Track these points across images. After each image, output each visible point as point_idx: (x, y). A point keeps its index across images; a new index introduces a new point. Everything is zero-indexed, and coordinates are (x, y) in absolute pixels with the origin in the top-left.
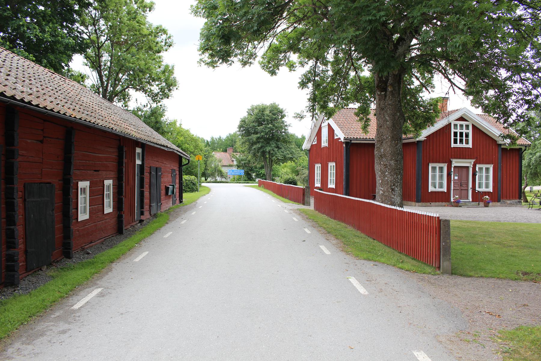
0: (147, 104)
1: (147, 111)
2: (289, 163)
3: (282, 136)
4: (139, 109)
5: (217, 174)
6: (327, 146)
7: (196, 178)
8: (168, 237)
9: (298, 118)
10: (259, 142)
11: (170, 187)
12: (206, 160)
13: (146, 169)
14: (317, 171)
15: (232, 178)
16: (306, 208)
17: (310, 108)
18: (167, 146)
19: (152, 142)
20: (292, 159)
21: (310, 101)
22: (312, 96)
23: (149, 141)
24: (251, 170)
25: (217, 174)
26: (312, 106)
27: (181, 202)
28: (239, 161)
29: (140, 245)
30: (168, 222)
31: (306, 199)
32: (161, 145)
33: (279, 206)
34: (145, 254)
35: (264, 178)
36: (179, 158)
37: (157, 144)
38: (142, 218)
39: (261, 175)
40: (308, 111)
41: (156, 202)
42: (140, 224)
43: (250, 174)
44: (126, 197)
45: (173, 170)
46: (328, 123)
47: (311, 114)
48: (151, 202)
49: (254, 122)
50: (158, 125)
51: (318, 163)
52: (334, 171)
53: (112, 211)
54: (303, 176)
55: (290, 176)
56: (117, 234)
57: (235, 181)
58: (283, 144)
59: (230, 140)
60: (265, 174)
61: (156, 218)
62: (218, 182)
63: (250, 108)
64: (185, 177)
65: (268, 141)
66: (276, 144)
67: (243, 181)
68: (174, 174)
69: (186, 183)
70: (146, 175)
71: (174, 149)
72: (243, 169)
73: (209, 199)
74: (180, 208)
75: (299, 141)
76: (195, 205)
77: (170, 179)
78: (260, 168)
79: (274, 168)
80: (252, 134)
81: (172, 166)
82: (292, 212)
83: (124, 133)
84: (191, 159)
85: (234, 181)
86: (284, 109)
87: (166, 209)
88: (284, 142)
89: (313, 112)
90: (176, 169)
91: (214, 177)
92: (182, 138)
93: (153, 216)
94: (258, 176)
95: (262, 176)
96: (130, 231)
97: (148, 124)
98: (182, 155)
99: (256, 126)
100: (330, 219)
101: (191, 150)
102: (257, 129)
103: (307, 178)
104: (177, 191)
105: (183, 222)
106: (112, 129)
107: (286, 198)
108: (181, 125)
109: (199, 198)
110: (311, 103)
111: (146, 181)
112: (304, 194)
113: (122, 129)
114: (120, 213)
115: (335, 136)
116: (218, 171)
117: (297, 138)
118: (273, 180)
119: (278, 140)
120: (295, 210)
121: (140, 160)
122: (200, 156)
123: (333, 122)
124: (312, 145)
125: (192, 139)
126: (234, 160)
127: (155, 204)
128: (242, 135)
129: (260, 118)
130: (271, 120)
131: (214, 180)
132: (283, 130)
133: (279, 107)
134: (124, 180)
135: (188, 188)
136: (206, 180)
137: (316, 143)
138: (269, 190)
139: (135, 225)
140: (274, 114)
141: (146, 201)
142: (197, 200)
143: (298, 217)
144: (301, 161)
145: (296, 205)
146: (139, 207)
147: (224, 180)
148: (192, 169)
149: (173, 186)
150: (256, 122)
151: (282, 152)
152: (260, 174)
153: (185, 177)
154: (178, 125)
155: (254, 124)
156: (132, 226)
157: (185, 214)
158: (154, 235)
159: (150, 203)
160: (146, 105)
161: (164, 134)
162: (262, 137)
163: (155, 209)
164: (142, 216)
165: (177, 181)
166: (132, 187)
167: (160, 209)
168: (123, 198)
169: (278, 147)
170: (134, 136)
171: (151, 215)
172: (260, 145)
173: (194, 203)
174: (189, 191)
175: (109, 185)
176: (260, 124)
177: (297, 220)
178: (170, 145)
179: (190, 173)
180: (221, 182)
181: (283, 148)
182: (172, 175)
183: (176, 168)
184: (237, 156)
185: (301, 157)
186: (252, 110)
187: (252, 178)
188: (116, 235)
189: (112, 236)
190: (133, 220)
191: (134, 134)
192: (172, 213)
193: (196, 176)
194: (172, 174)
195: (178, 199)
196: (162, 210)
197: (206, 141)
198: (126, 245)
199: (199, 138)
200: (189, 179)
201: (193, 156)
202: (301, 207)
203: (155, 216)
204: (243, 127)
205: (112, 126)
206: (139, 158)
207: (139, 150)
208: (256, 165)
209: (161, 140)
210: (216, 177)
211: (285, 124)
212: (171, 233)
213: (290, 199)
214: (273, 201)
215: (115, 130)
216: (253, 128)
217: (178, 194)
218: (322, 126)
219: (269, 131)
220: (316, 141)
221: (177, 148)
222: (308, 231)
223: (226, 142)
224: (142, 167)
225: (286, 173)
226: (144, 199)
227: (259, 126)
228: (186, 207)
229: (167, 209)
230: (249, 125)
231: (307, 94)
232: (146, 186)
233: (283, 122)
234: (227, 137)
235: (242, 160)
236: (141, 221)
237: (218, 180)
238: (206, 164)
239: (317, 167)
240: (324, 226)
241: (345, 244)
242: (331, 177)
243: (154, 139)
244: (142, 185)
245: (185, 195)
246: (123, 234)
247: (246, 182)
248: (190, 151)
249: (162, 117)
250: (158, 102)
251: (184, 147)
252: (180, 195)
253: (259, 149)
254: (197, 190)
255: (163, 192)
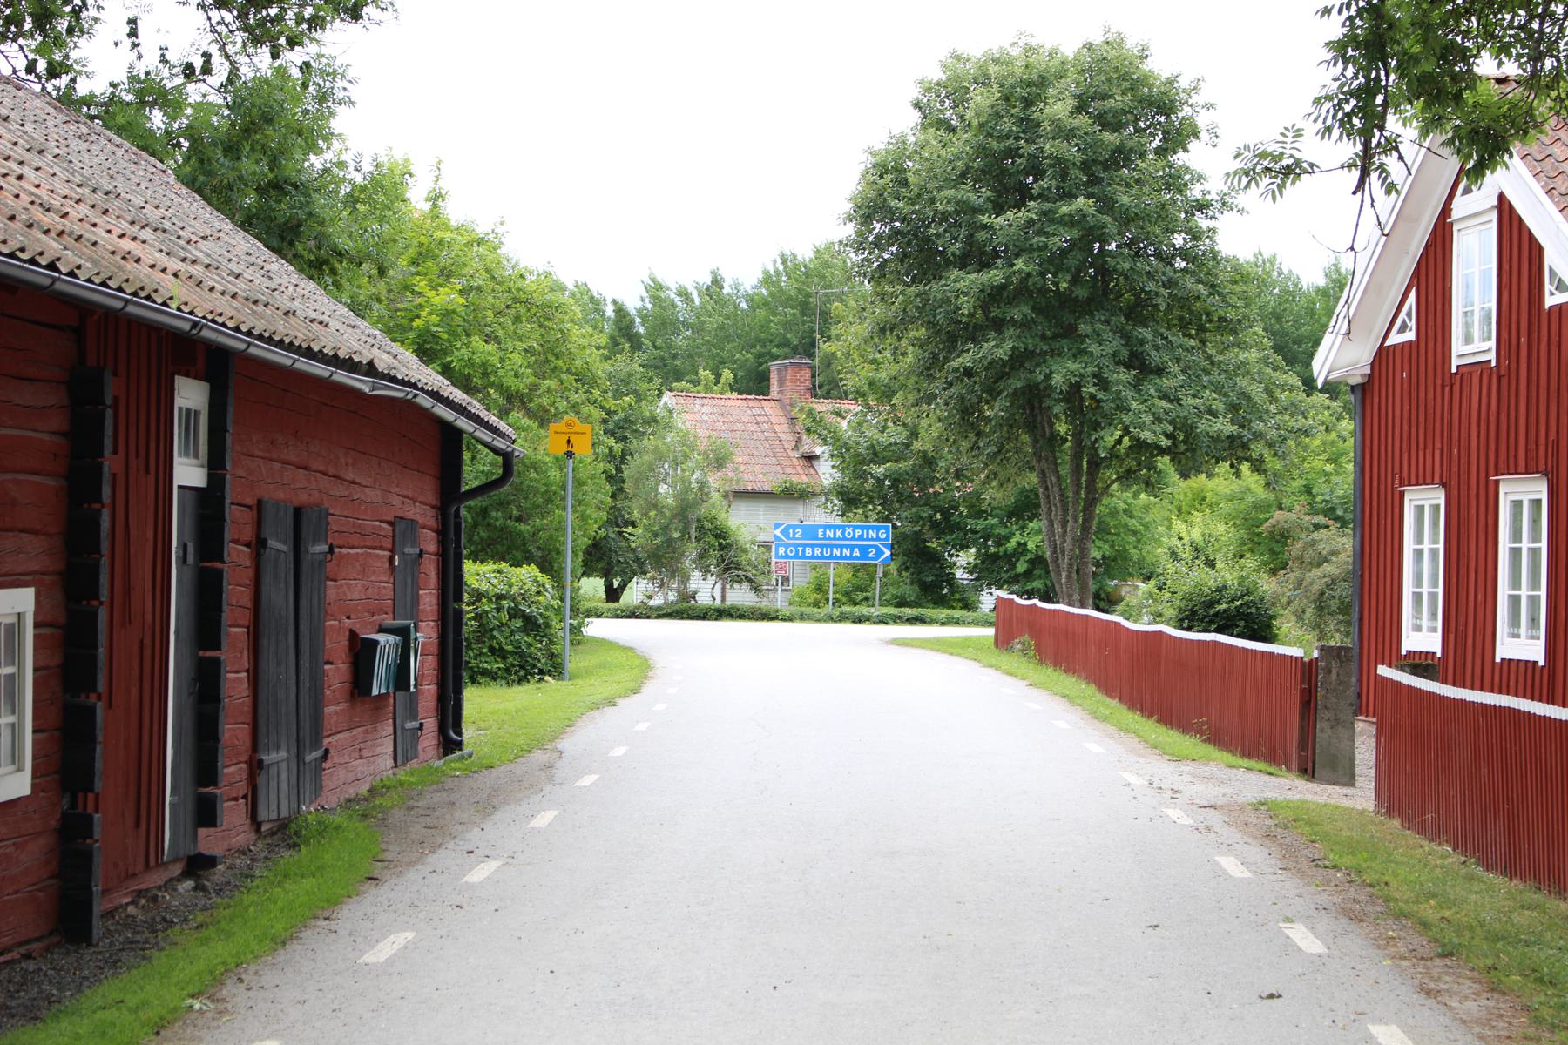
0: (207, 56)
1: (203, 107)
2: (1220, 482)
3: (1170, 284)
4: (149, 93)
5: (692, 550)
6: (1492, 356)
7: (545, 579)
8: (390, 961)
9: (1266, 180)
10: (999, 325)
11: (382, 638)
12: (618, 448)
13: (237, 522)
14: (1419, 540)
15: (801, 579)
16: (1321, 799)
17: (1348, 108)
18: (371, 364)
19: (280, 344)
20: (1245, 446)
21: (1346, 61)
22: (1359, 22)
23: (260, 337)
24: (949, 525)
25: (692, 550)
26: (1357, 93)
27: (449, 743)
28: (856, 460)
29: (221, 1006)
30: (377, 870)
31: (1324, 733)
32: (335, 361)
33: (1132, 779)
34: (403, 938)
35: (1037, 584)
36: (449, 442)
37: (309, 353)
38: (208, 841)
39: (1021, 567)
40: (1329, 129)
41: (293, 741)
42: (189, 884)
43: (934, 558)
44: (110, 705)
45: (400, 527)
46: (1501, 197)
47: (1350, 149)
48: (262, 741)
49: (963, 175)
50: (284, 209)
51: (1421, 480)
52: (1535, 538)
53: (27, 791)
54: (1316, 578)
55: (1227, 575)
56: (55, 939)
57: (829, 609)
58: (1177, 338)
59: (788, 301)
60: (1048, 555)
61: (295, 846)
62: (703, 615)
63: (937, 75)
64: (478, 574)
65: (1068, 318)
66: (1126, 337)
67: (887, 603)
68: (409, 550)
69: (478, 617)
70: (237, 555)
71: (414, 386)
72: (886, 519)
73: (642, 726)
74: (449, 784)
75: (1311, 313)
76: (549, 767)
77: (380, 585)
78: (1010, 515)
79: (1114, 513)
80: (948, 264)
81: (396, 501)
82: (1215, 818)
83: (120, 289)
84: (519, 447)
85: (816, 604)
86: (1184, 83)
87: (351, 792)
88: (1184, 326)
89: (1366, 134)
90: (421, 520)
91: (673, 574)
92: (447, 296)
93: (272, 833)
94: (993, 569)
95: (1028, 574)
96: (129, 923)
97: (218, 195)
98: (463, 424)
99: (977, 210)
100: (1480, 871)
101: (510, 382)
102: (986, 227)
103: (1344, 590)
104: (422, 665)
105: (479, 874)
106: (52, 266)
107: (1185, 727)
108: (436, 198)
109: (569, 724)
110: (1350, 71)
111: (236, 594)
112: (1308, 704)
113: (109, 265)
114: (74, 805)
115: (1548, 287)
116: (701, 529)
117: (1291, 294)
118: (1105, 601)
119: (1139, 311)
120: (1242, 808)
121: (196, 456)
122: (579, 426)
123: (1537, 188)
124: (1384, 355)
125: (516, 300)
126: (818, 450)
127: (283, 754)
128: (880, 275)
129: (1013, 153)
130: (1085, 166)
131: (672, 597)
132: (1178, 240)
133: (1149, 65)
134: (104, 595)
135: (492, 649)
136: (613, 594)
137: (1410, 336)
138: (1070, 669)
139: (159, 888)
140: (1109, 122)
141: (233, 732)
142: (557, 735)
143: (1257, 853)
144: (1319, 463)
145: (1252, 777)
146: (188, 773)
147: (740, 596)
148: (519, 519)
149: (403, 632)
150: (982, 175)
151: (1165, 397)
152: (1011, 558)
153: (478, 574)
154: (417, 197)
155: (965, 193)
156: (140, 893)
157: (487, 825)
158: (295, 946)
159: (255, 748)
160: (198, 63)
161: (333, 272)
162: (1021, 291)
163: (284, 786)
164: (202, 832)
165: (429, 600)
166: (147, 641)
167: (319, 788)
168: (100, 706)
169: (1141, 366)
170: (174, 304)
171: (258, 830)
172: (1008, 345)
173: (539, 757)
174: (494, 677)
175: (14, 619)
176: (1010, 194)
177: (1247, 874)
178: (389, 359)
179: (509, 549)
180: (722, 613)
181: (1175, 369)
182: (391, 560)
183: (422, 513)
184: (844, 424)
185: (1306, 433)
186: (955, 91)
187: (951, 581)
188: (47, 949)
189: (23, 950)
190: (152, 857)
191: (175, 292)
192: (397, 815)
193: (548, 565)
194: (393, 551)
195: (431, 724)
196: (330, 799)
197: (610, 311)
198: (131, 1001)
199: (561, 288)
200: (501, 588)
201: (526, 422)
202: (1289, 788)
203: (286, 834)
204: (889, 214)
205: (53, 247)
206: (191, 450)
207: (190, 395)
208: (977, 495)
209: (334, 325)
210: (685, 579)
211: (1195, 192)
212: (410, 935)
213: (1217, 738)
214: (1095, 748)
215: (71, 274)
216: (957, 225)
217: (429, 690)
218: (1455, 215)
219: (1073, 244)
220: (1413, 324)
221: (409, 365)
222: (1305, 939)
223: (762, 313)
224: (208, 501)
225: (1202, 555)
226: (222, 716)
227: (999, 209)
228: (485, 780)
229: (364, 789)
230: (933, 201)
231: (1327, 11)
232: (235, 633)
233: (1175, 181)
234: (767, 280)
235: (876, 455)
236: (198, 865)
237: (704, 599)
238: (615, 479)
239: (1420, 509)
240: (1429, 911)
241: (1538, 1021)
242: (1515, 583)
243: (291, 319)
244: (206, 629)
245: (479, 702)
246: (90, 944)
247: (909, 612)
248: (500, 387)
249: (312, 148)
250: (282, 41)
251: (458, 356)
252: (442, 698)
253: (1000, 371)
254: (556, 668)
255: (337, 674)
